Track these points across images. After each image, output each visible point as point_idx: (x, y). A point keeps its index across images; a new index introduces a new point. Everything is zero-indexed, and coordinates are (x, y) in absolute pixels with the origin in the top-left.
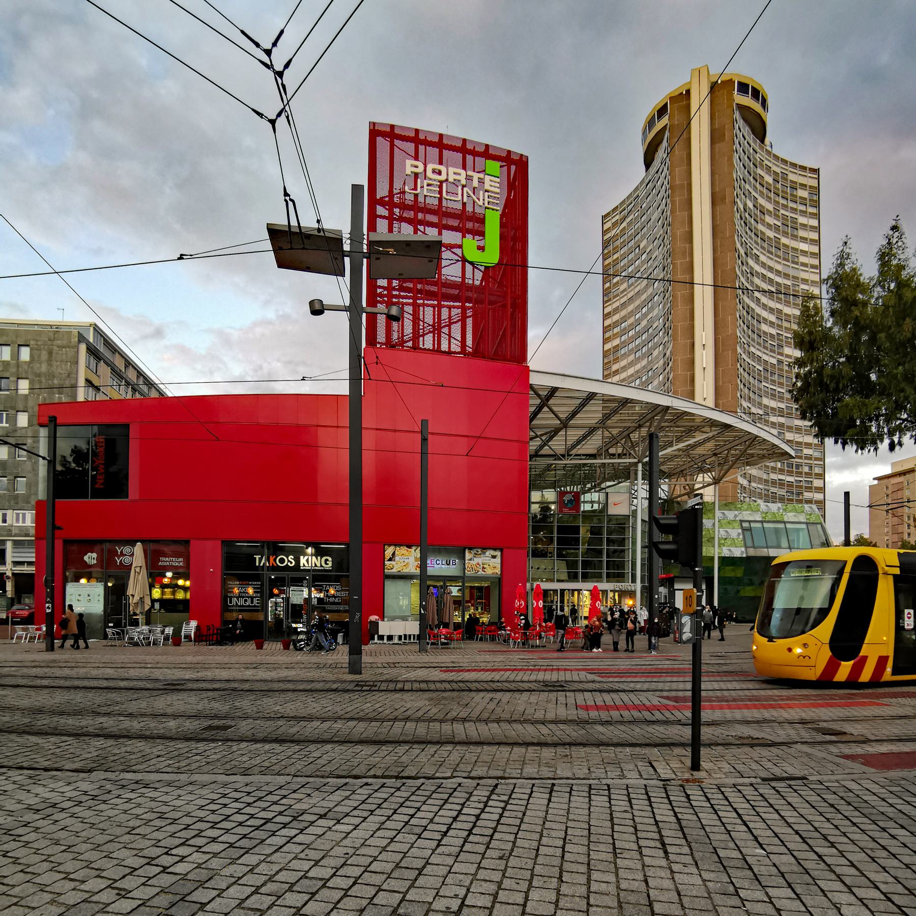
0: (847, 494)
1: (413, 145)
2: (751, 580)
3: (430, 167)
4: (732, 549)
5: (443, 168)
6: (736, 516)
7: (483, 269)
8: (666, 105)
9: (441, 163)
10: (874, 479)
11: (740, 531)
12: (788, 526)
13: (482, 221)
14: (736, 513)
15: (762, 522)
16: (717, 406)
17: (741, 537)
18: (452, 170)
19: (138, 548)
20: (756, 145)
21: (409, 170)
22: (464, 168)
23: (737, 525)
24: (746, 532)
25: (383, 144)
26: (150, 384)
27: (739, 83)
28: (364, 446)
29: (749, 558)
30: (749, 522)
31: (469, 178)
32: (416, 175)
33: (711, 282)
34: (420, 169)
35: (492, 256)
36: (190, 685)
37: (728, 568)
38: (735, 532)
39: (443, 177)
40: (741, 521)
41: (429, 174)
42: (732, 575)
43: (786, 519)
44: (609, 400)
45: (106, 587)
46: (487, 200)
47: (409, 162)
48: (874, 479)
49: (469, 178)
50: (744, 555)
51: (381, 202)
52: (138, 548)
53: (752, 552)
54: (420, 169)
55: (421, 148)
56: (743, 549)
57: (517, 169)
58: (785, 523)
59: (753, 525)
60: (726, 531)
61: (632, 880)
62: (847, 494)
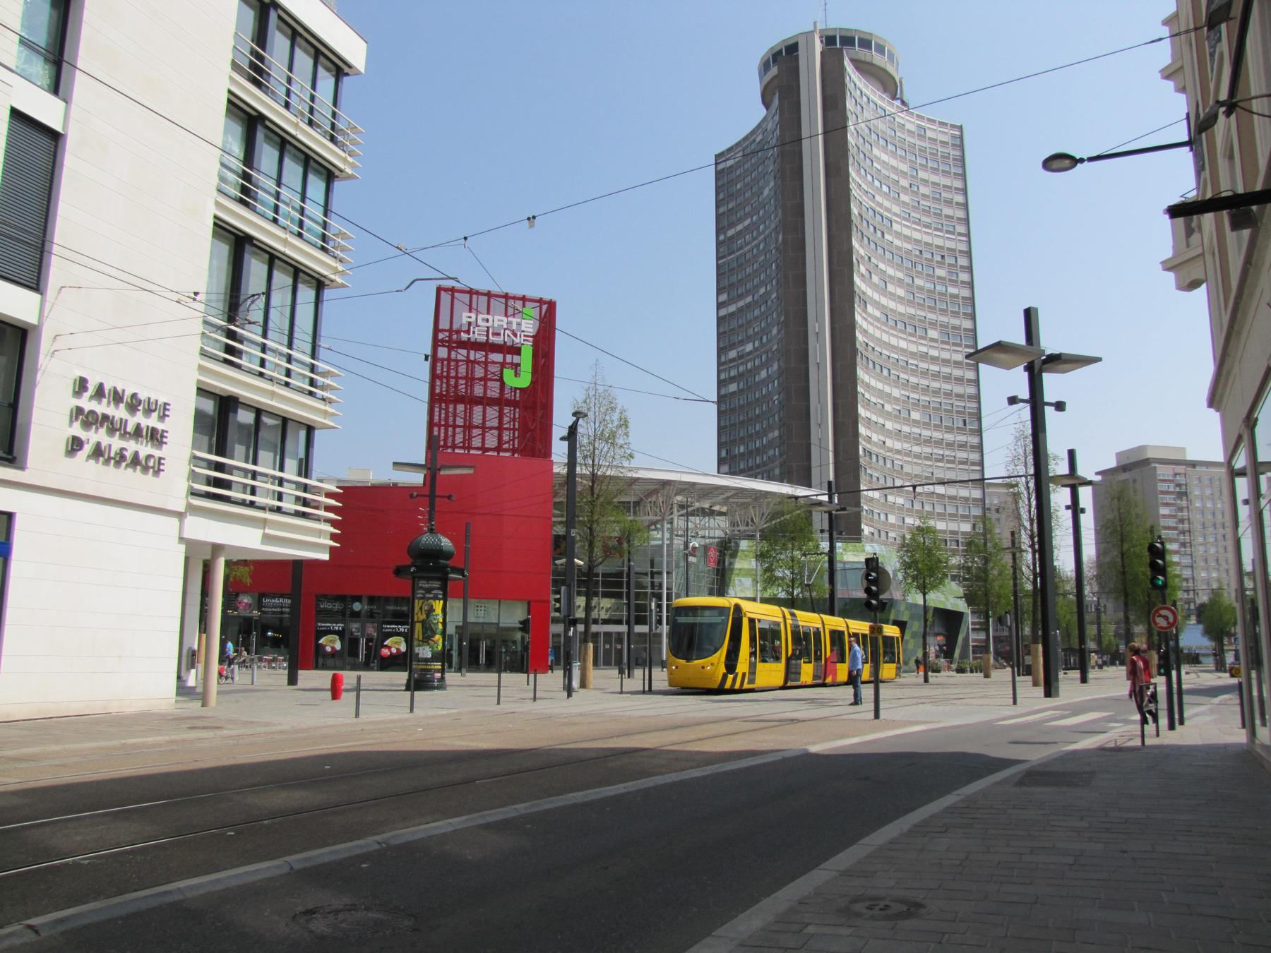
0: (1015, 703)
3: (480, 317)
5: (490, 317)
8: (780, 51)
9: (488, 313)
18: (496, 318)
20: (892, 107)
21: (465, 320)
22: (506, 315)
25: (446, 297)
27: (860, 40)
31: (509, 323)
32: (470, 324)
34: (473, 320)
35: (525, 380)
39: (489, 324)
41: (480, 322)
44: (750, 469)
45: (513, 629)
47: (465, 314)
49: (509, 323)
51: (441, 378)
54: (473, 320)
55: (475, 297)
57: (548, 314)
62: (1015, 703)
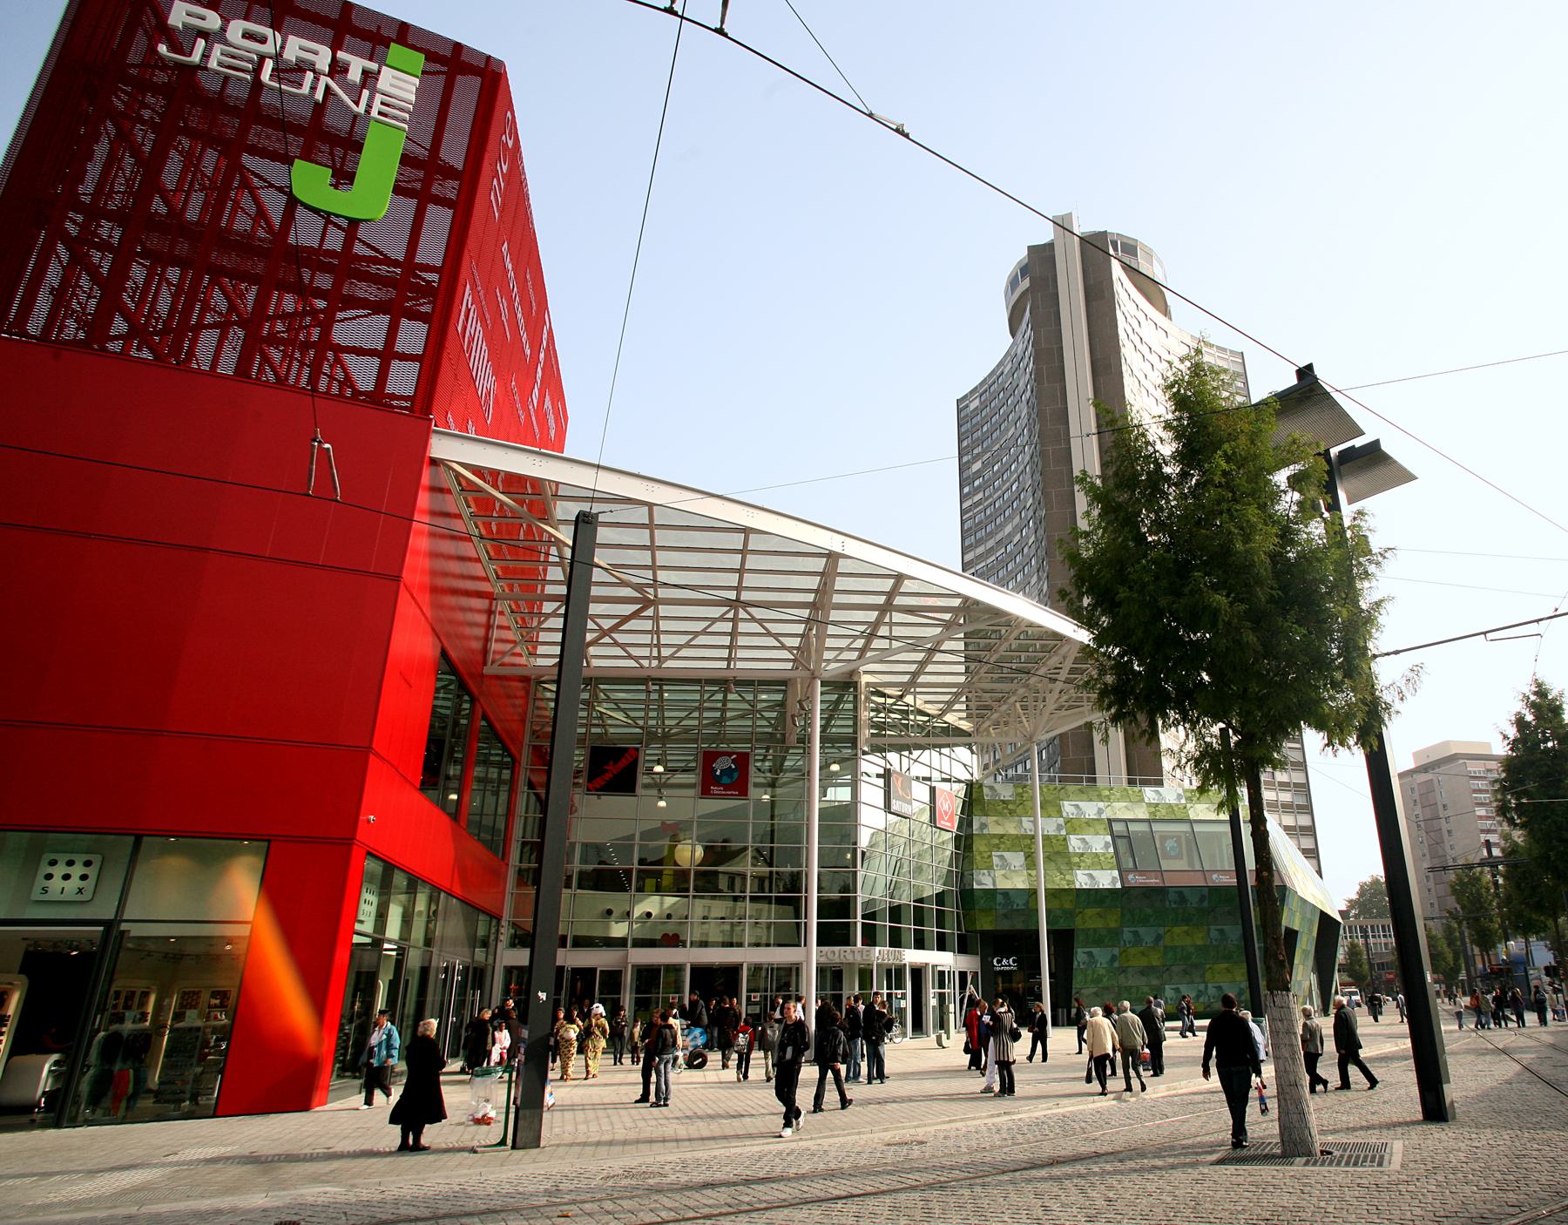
1: (396, 365)
2: (1136, 933)
4: (1095, 873)
6: (1100, 811)
7: (345, 224)
11: (1109, 838)
12: (1197, 828)
13: (353, 145)
14: (1101, 805)
15: (1148, 821)
16: (1401, 776)
17: (1111, 850)
19: (255, 288)
23: (1101, 828)
24: (1119, 841)
29: (1126, 891)
30: (1126, 821)
33: (1094, 430)
37: (1089, 912)
38: (1100, 843)
40: (1110, 821)
42: (1099, 924)
43: (1192, 817)
46: (377, 106)
50: (1119, 886)
52: (255, 288)
53: (1134, 880)
56: (1116, 873)
58: (1191, 822)
59: (1133, 827)
60: (1083, 840)
61: (490, 799)
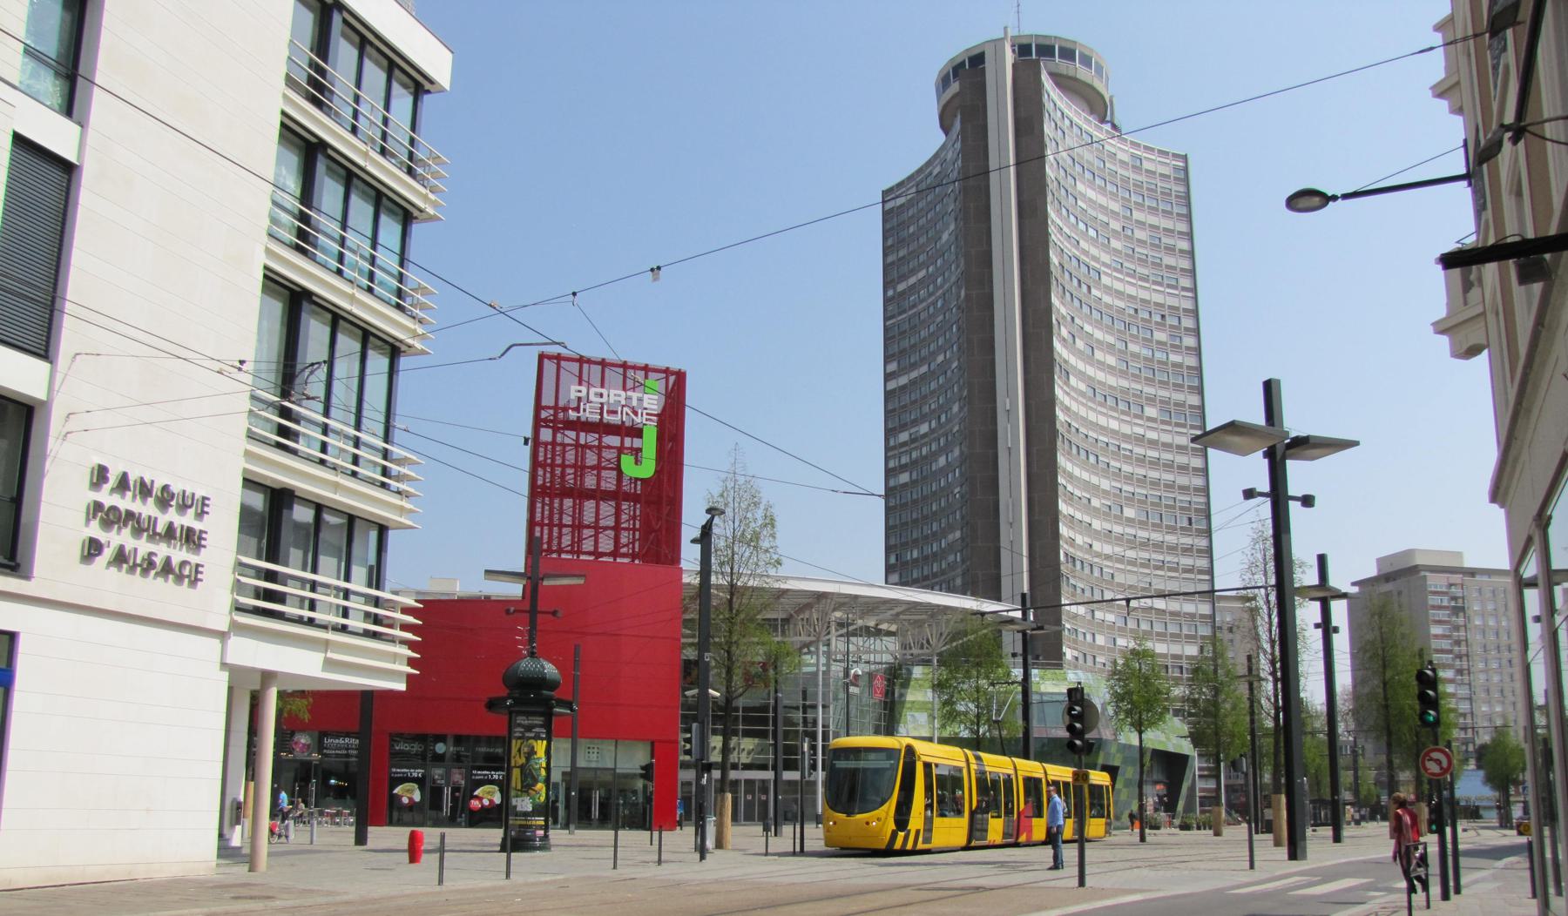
5: (604, 391)
9: (602, 386)
10: (1354, 584)
18: (612, 392)
21: (573, 395)
22: (624, 389)
25: (550, 367)
26: (594, 805)
28: (655, 430)
31: (628, 398)
32: (579, 399)
35: (647, 469)
36: (330, 152)
39: (604, 400)
41: (592, 397)
45: (633, 776)
47: (574, 388)
48: (1354, 584)
49: (628, 398)
51: (544, 466)
54: (584, 394)
57: (676, 387)
